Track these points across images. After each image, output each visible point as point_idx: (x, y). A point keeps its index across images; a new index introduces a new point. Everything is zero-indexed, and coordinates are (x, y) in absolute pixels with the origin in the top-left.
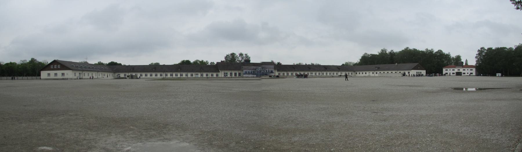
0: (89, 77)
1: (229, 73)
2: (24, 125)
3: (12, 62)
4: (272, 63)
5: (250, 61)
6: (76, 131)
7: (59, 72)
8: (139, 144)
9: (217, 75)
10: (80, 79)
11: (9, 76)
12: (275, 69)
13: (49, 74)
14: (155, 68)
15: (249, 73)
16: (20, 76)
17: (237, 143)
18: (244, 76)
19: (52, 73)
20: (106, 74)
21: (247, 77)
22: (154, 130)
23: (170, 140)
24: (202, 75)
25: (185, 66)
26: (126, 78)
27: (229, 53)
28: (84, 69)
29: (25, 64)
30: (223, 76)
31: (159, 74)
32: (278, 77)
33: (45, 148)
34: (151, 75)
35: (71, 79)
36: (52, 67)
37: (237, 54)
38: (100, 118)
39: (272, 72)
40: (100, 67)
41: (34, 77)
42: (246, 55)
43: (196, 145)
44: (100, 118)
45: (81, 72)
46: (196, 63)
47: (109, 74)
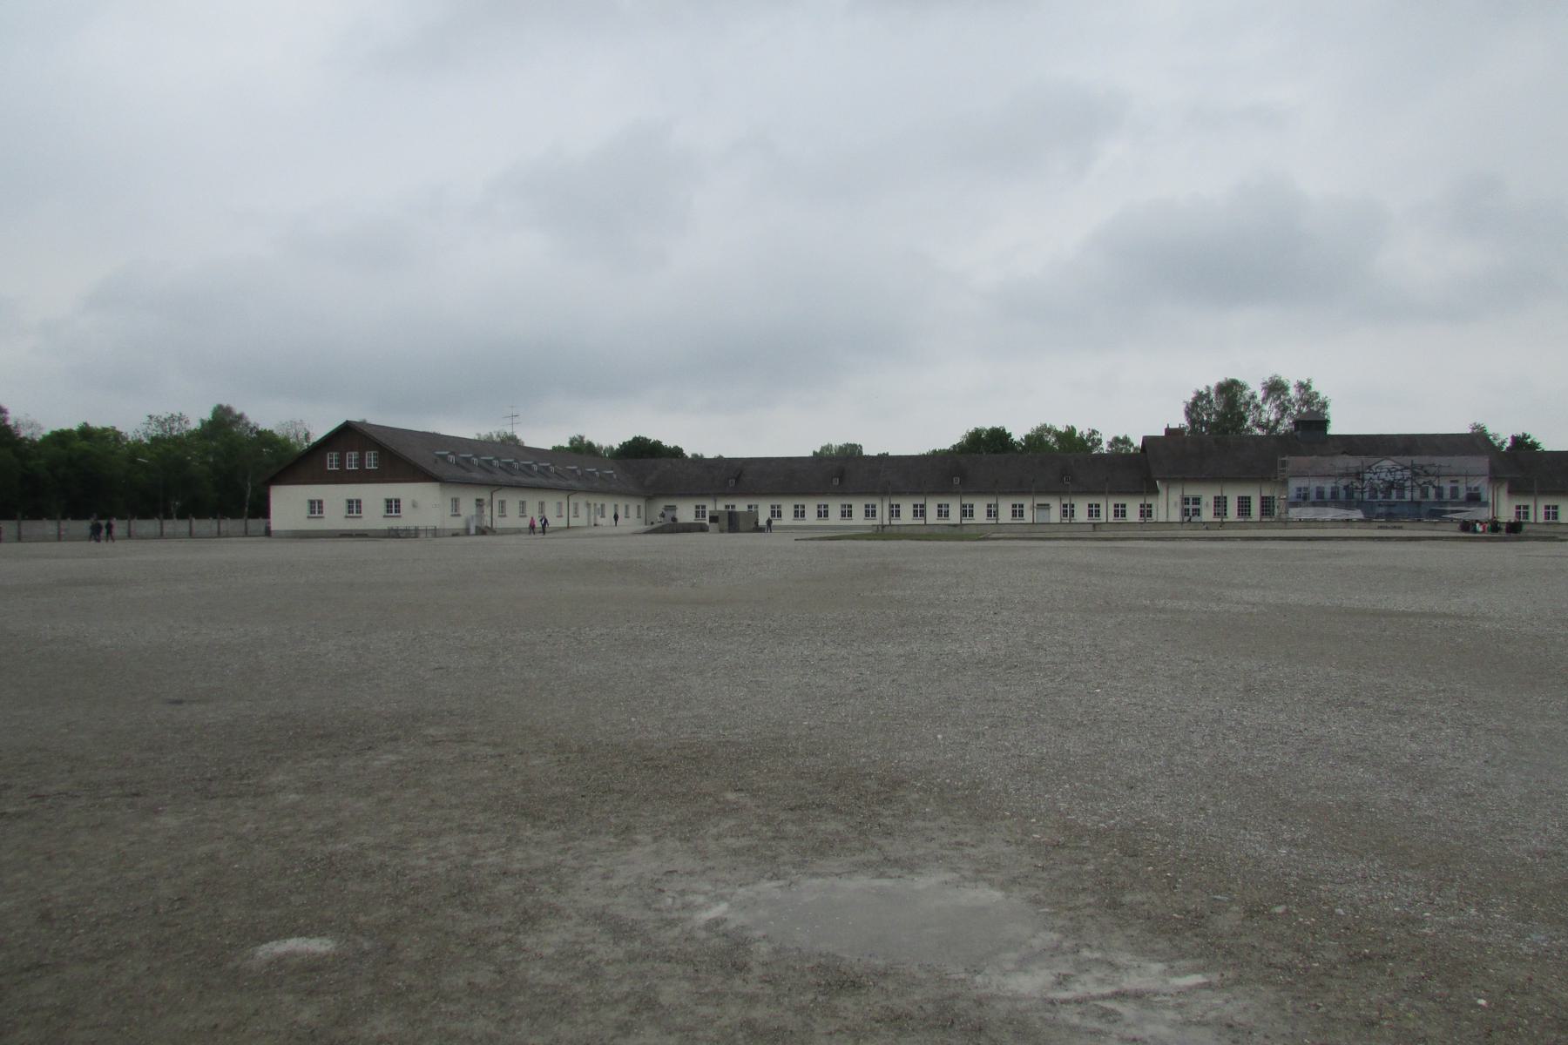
0: (525, 523)
1: (1208, 495)
2: (169, 821)
3: (96, 423)
4: (1477, 442)
5: (1324, 423)
6: (464, 829)
7: (373, 495)
8: (767, 886)
9: (1146, 512)
10: (482, 531)
11: (77, 513)
12: (1495, 478)
13: (316, 507)
14: (842, 475)
15: (1321, 501)
16: (145, 516)
17: (1251, 912)
18: (1294, 513)
19: (334, 496)
20: (610, 504)
21: (1307, 523)
22: (835, 810)
23: (910, 866)
24: (1068, 511)
25: (985, 462)
26: (702, 529)
27: (1209, 380)
28: (502, 477)
29: (178, 441)
30: (1176, 515)
31: (858, 507)
32: (1514, 528)
33: (294, 944)
34: (823, 513)
35: (436, 533)
36: (331, 461)
37: (1255, 387)
38: (582, 750)
39: (1474, 499)
40: (578, 468)
41: (228, 524)
42: (1303, 387)
43: (1036, 902)
44: (582, 750)
45: (484, 495)
46: (1036, 441)
47: (622, 504)
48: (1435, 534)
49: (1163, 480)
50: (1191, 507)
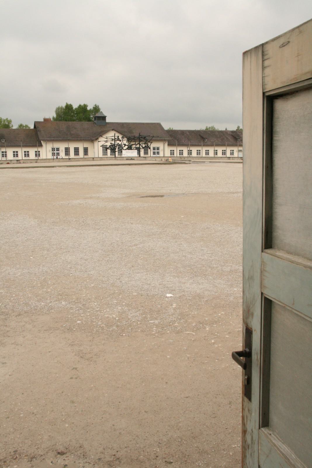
1: (62, 146)
9: (37, 154)
30: (50, 156)
48: (220, 161)
49: (44, 140)
50: (56, 152)
